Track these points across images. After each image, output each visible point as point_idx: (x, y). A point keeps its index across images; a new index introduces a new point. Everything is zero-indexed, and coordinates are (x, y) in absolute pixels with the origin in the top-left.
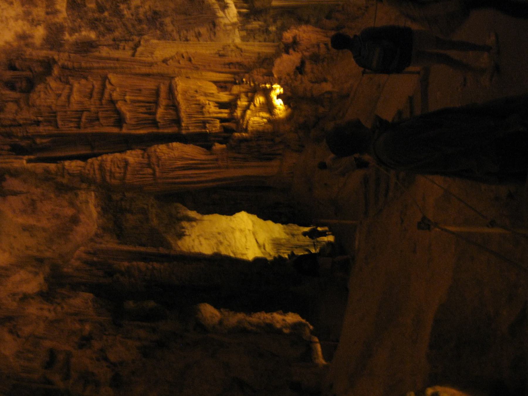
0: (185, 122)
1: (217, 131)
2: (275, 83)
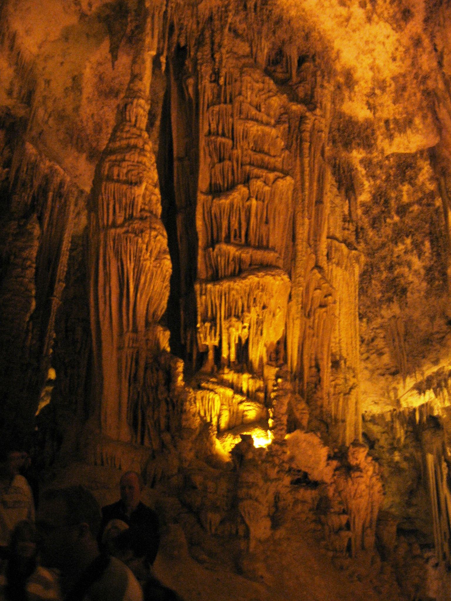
0: (212, 289)
1: (199, 341)
2: (275, 434)
